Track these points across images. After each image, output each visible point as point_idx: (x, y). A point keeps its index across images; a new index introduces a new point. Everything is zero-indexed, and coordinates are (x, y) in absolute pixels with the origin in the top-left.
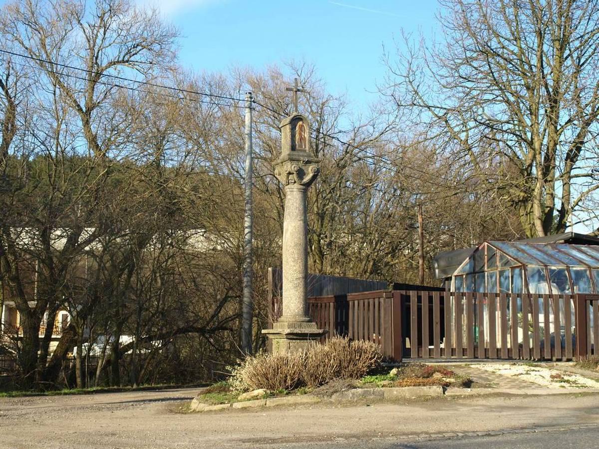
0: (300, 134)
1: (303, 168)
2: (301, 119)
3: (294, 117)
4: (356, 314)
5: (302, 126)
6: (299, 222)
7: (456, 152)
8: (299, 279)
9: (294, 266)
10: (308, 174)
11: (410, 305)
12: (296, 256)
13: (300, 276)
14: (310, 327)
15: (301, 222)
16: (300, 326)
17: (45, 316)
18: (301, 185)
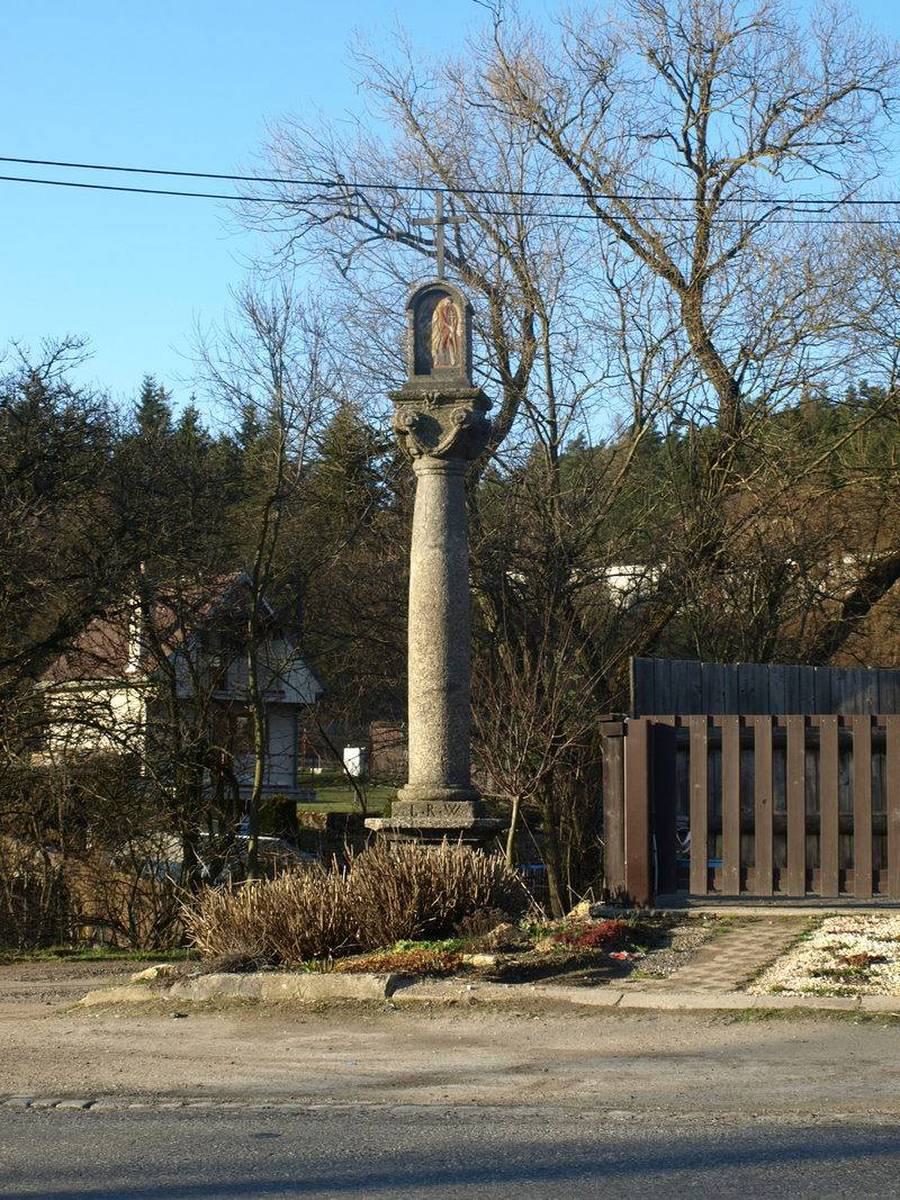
0: (444, 329)
1: (435, 415)
2: (444, 294)
3: (421, 289)
4: (796, 784)
5: (449, 309)
6: (432, 552)
7: (535, 362)
8: (429, 692)
9: (420, 660)
10: (450, 428)
11: (786, 736)
12: (423, 636)
13: (434, 685)
14: (454, 812)
15: (437, 551)
16: (428, 810)
17: (606, 969)
18: (435, 457)
